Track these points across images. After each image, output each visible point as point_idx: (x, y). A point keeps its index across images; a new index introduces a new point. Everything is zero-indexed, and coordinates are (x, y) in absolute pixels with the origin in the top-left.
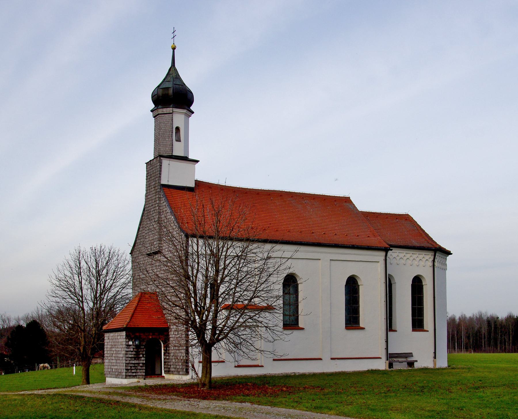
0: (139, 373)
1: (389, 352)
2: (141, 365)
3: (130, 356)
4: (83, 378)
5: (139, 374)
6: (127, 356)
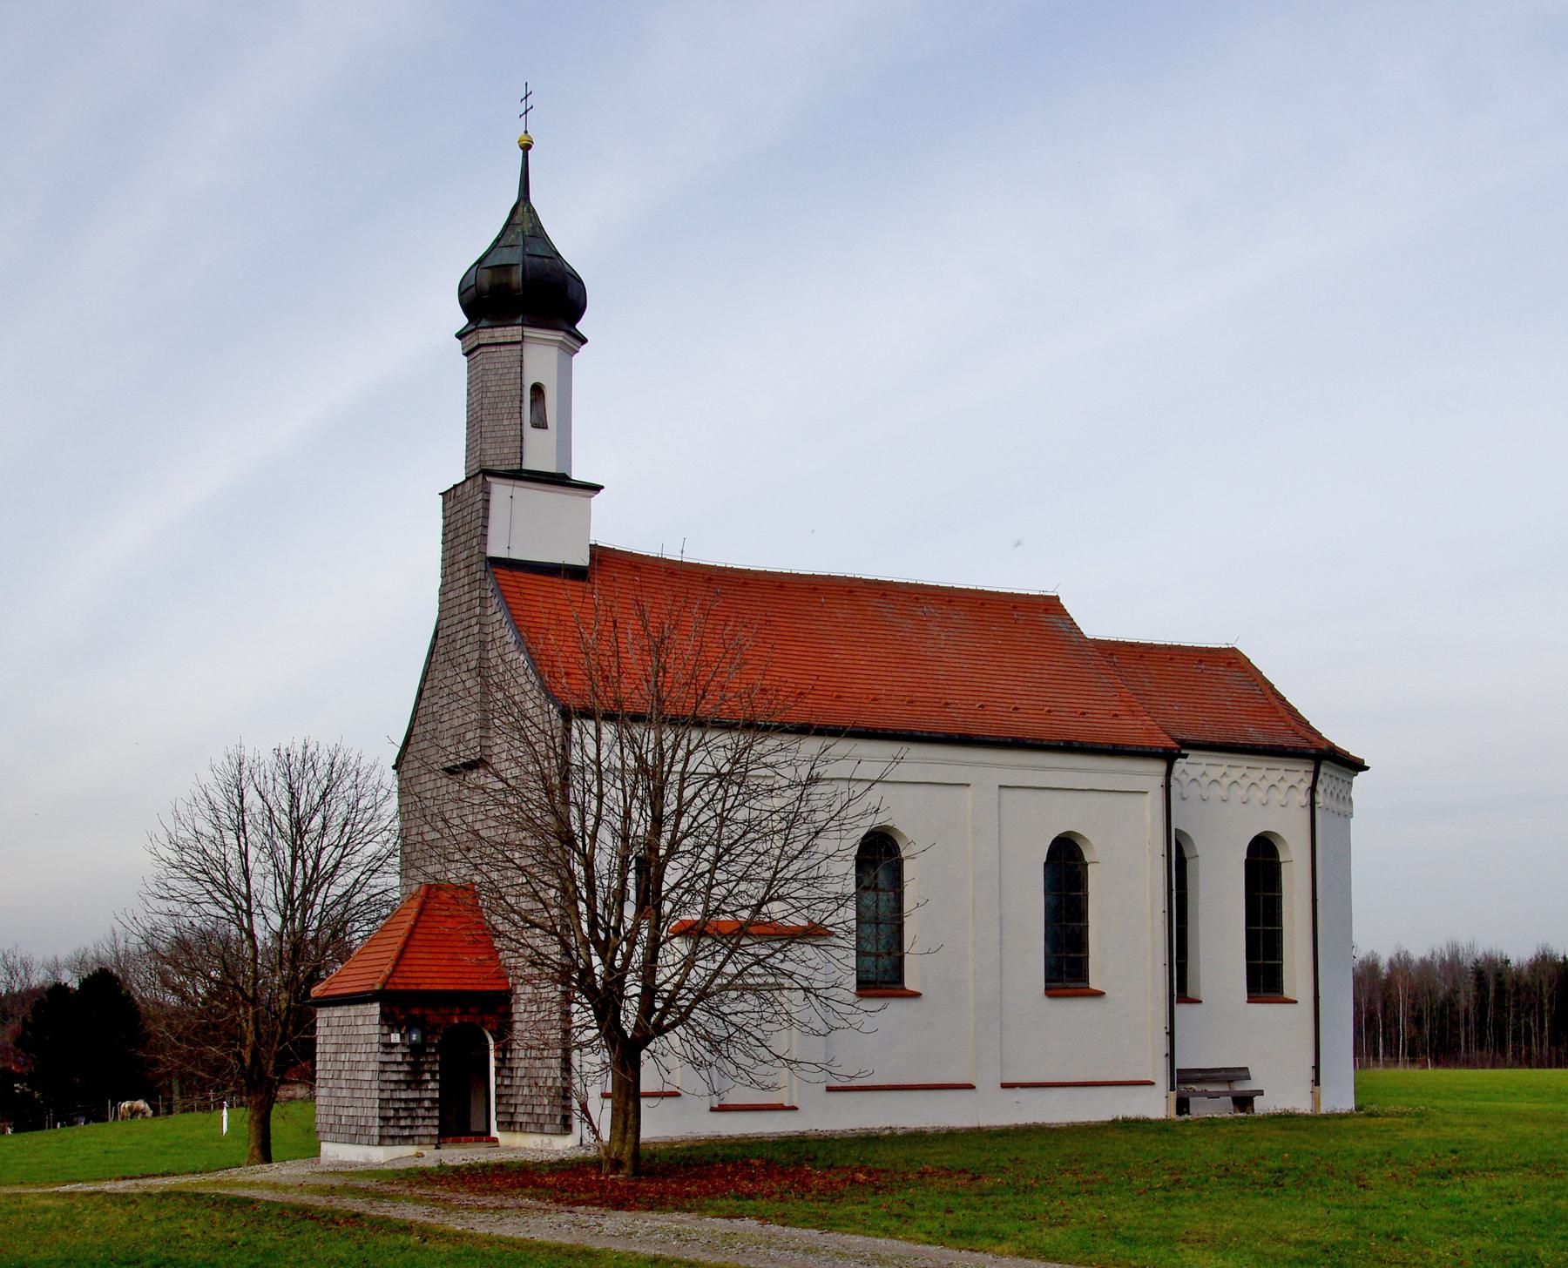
0: (420, 1129)
1: (1179, 1065)
2: (427, 1104)
3: (395, 1077)
4: (252, 1145)
5: (421, 1131)
6: (386, 1076)
